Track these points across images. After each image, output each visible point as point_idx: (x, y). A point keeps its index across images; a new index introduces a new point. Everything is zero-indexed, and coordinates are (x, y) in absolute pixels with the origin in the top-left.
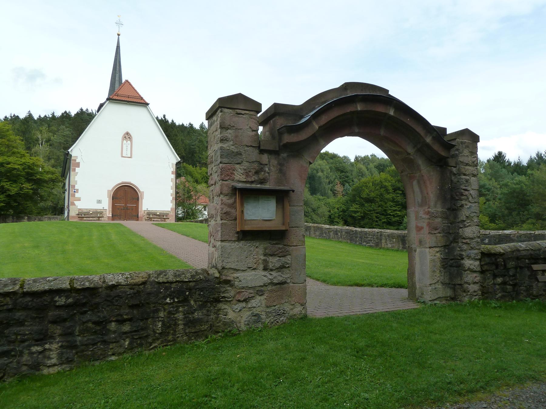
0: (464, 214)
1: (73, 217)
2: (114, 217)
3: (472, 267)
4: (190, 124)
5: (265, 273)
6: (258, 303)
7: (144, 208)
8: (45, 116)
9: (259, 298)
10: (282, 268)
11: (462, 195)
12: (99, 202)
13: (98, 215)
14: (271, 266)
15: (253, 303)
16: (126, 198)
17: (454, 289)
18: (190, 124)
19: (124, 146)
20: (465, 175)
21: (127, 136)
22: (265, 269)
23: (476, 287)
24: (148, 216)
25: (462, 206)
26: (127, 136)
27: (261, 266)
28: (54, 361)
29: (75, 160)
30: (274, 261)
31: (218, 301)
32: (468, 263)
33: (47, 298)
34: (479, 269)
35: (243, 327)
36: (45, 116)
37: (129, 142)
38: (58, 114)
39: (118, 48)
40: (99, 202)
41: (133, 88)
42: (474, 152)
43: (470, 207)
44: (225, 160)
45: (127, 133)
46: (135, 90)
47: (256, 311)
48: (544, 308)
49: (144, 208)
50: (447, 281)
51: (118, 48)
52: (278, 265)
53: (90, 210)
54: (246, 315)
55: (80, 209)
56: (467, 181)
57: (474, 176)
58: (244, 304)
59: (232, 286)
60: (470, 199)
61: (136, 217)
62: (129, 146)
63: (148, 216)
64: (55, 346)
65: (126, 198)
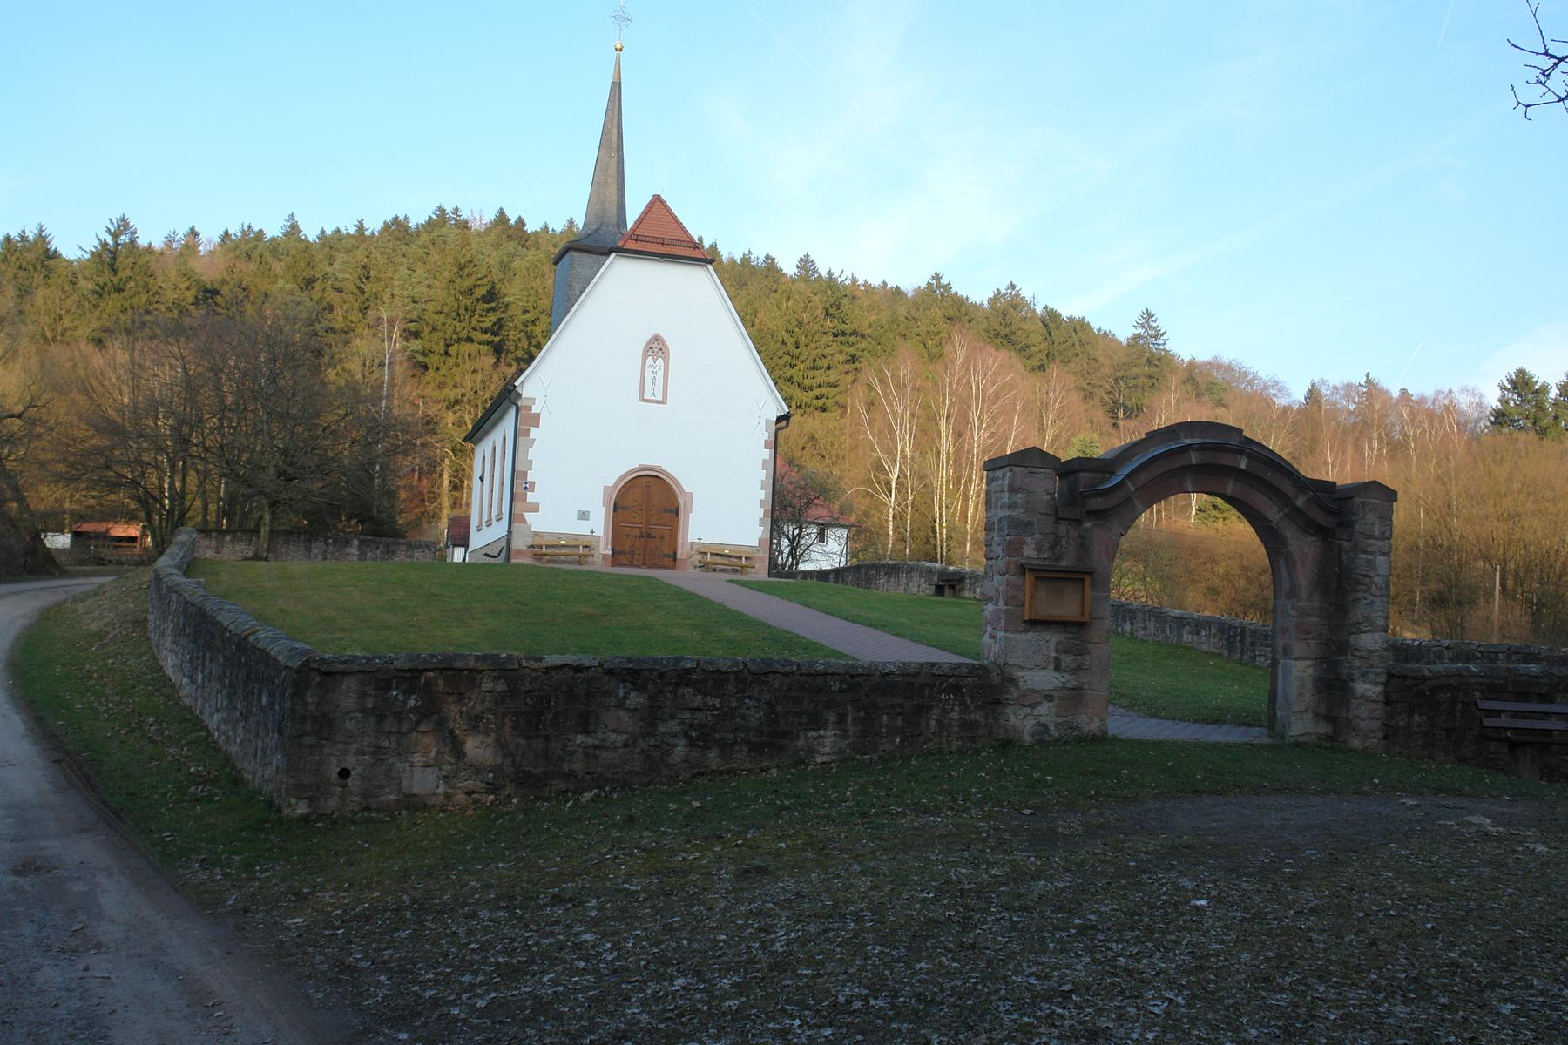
0: (1357, 613)
1: (519, 552)
2: (617, 556)
3: (1369, 694)
4: (768, 257)
5: (1057, 674)
6: (1045, 711)
7: (692, 537)
8: (338, 231)
9: (1046, 704)
10: (1079, 668)
11: (1358, 583)
12: (583, 516)
13: (579, 549)
14: (1064, 666)
15: (1041, 710)
16: (647, 505)
17: (1332, 720)
18: (768, 257)
19: (649, 372)
20: (1365, 552)
21: (656, 347)
22: (1057, 668)
23: (1376, 725)
24: (699, 557)
25: (1357, 600)
26: (656, 347)
27: (1052, 666)
28: (827, 749)
29: (530, 408)
30: (1067, 660)
31: (998, 702)
32: (1361, 687)
33: (819, 680)
34: (1382, 698)
35: (1027, 739)
36: (338, 231)
37: (660, 361)
38: (374, 225)
39: (616, 87)
40: (583, 516)
41: (674, 217)
42: (1386, 517)
43: (1372, 602)
44: (1013, 532)
45: (656, 338)
46: (680, 224)
47: (1043, 720)
48: (32, 259)
49: (692, 537)
50: (1323, 711)
51: (616, 87)
52: (1073, 666)
53: (560, 536)
54: (1030, 724)
55: (537, 534)
56: (1369, 562)
57: (1383, 554)
58: (1028, 710)
59: (1017, 685)
60: (1374, 589)
61: (671, 560)
62: (660, 373)
63: (699, 557)
64: (829, 733)
65: (647, 505)
